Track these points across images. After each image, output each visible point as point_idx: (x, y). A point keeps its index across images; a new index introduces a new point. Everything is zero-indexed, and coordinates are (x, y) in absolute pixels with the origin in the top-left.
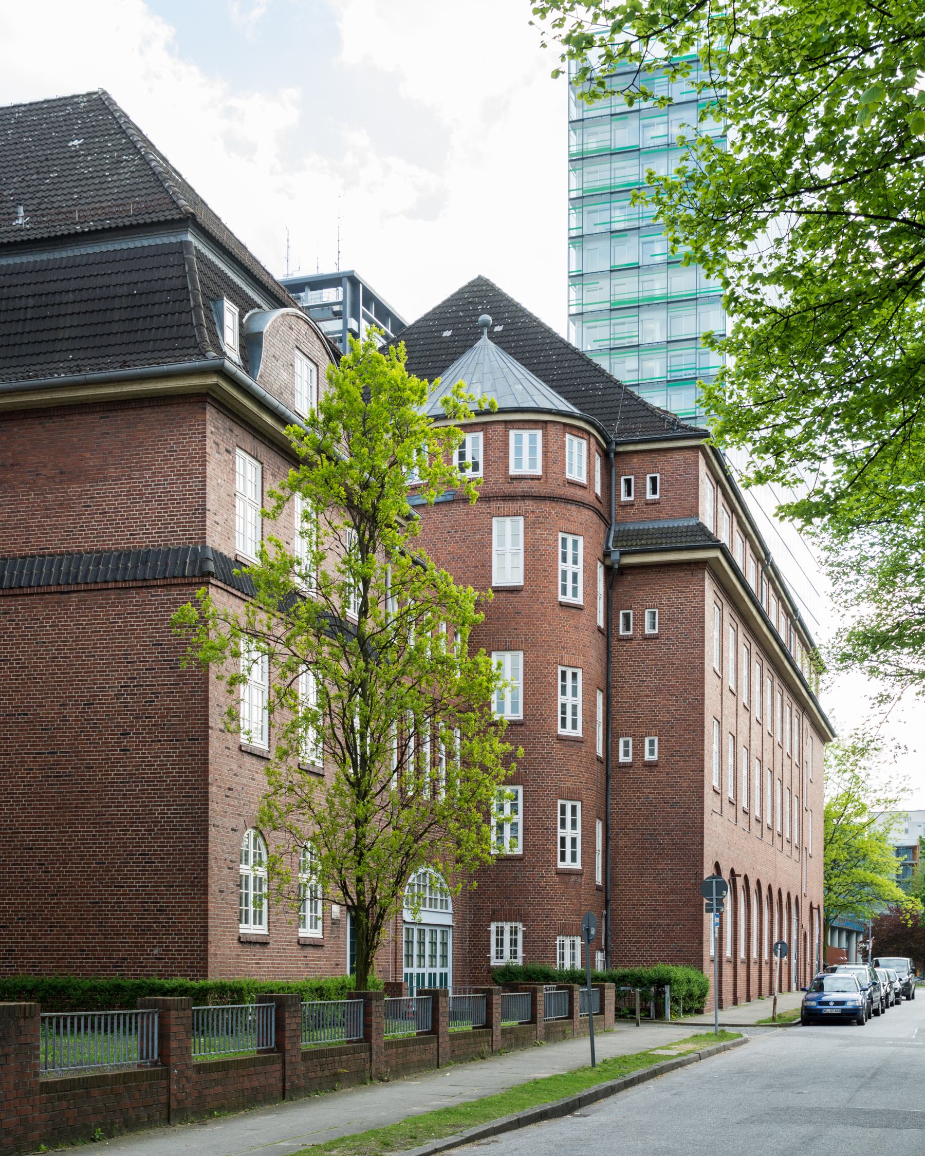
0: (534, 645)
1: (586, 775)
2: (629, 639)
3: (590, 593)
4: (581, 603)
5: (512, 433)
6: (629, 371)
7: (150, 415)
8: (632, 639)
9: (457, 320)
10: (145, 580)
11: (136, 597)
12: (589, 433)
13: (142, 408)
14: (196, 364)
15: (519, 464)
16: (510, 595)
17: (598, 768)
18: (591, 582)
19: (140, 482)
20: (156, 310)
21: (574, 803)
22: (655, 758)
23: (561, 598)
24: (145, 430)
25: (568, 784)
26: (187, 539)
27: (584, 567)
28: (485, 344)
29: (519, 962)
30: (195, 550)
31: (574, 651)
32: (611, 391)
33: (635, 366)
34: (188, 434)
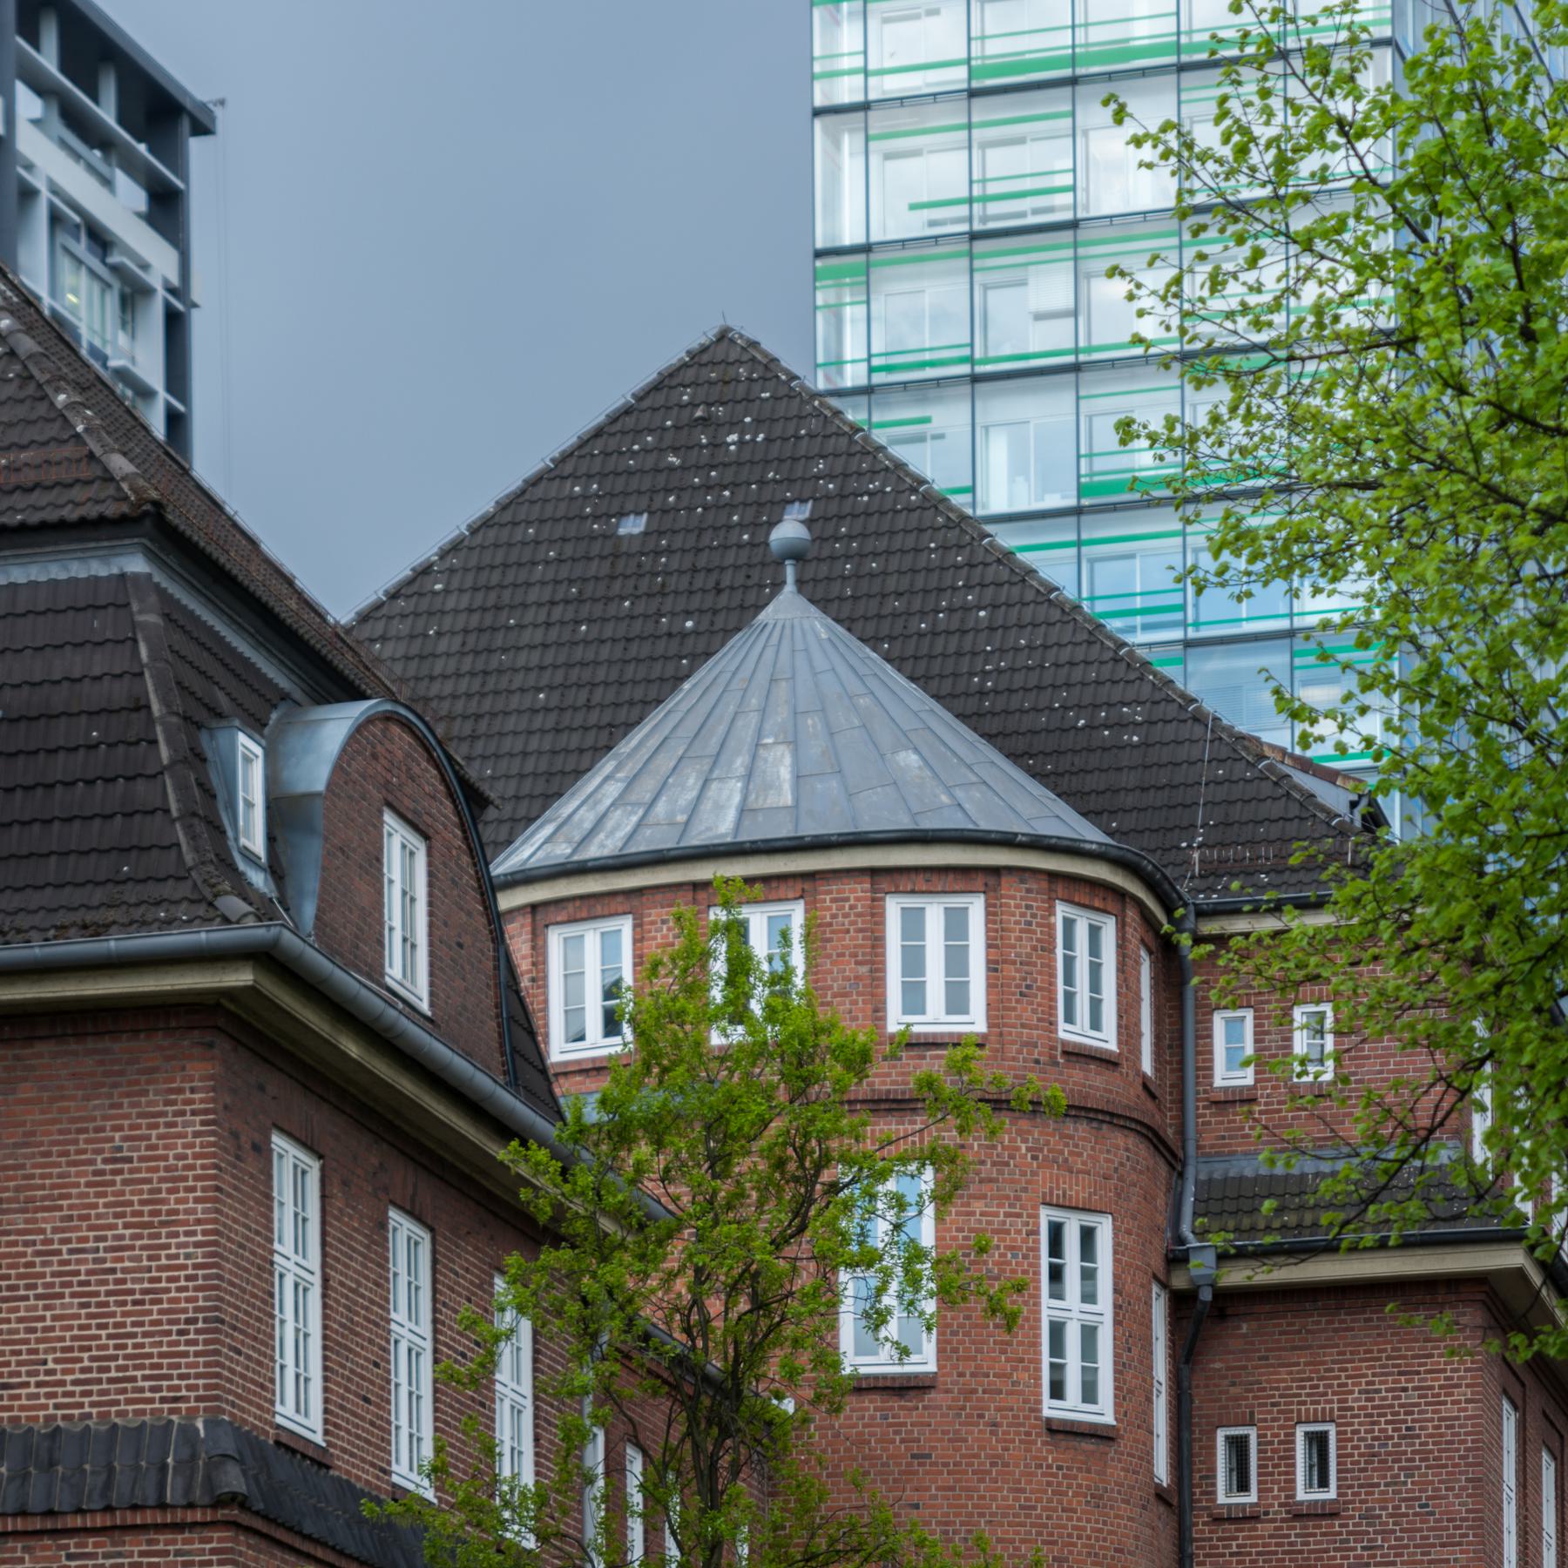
2: (1250, 1517)
3: (1132, 1390)
4: (1109, 1419)
5: (894, 907)
6: (1039, 317)
7: (48, 1058)
8: (1255, 1518)
9: (661, 480)
10: (50, 1513)
12: (1121, 895)
13: (31, 1040)
14: (202, 937)
15: (914, 998)
16: (895, 1403)
18: (1135, 1351)
19: (26, 1244)
20: (60, 767)
23: (1050, 1409)
24: (39, 1101)
26: (163, 1400)
27: (1117, 1307)
28: (788, 609)
30: (188, 1431)
32: (1170, 731)
33: (1064, 300)
34: (163, 1114)
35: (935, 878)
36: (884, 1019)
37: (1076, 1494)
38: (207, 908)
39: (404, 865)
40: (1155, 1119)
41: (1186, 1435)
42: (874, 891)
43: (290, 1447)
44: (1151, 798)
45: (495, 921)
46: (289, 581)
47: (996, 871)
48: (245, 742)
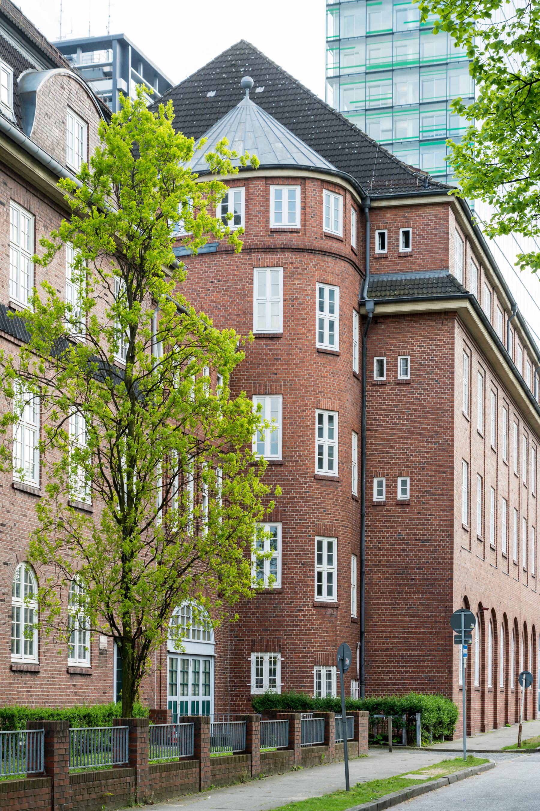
0: (292, 389)
1: (342, 513)
2: (383, 384)
3: (346, 341)
4: (337, 350)
5: (273, 189)
8: (385, 385)
9: (221, 81)
12: (345, 189)
15: (279, 218)
16: (270, 342)
17: (353, 506)
18: (347, 330)
21: (331, 540)
22: (407, 497)
23: (318, 345)
25: (325, 522)
28: (247, 104)
29: (278, 690)
31: (330, 396)
32: (366, 149)
33: (389, 127)
35: (285, 180)
36: (269, 223)
37: (326, 372)
41: (364, 359)
42: (266, 184)
44: (360, 168)
46: (32, 26)
47: (304, 178)
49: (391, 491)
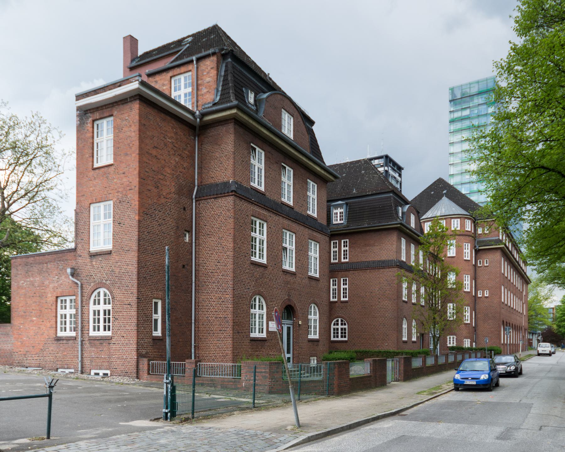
5: (452, 220)
11: (382, 270)
17: (473, 298)
22: (488, 295)
23: (465, 259)
29: (455, 345)
38: (396, 220)
39: (413, 218)
40: (473, 236)
43: (403, 261)
45: (420, 223)
48: (400, 208)
49: (483, 294)
